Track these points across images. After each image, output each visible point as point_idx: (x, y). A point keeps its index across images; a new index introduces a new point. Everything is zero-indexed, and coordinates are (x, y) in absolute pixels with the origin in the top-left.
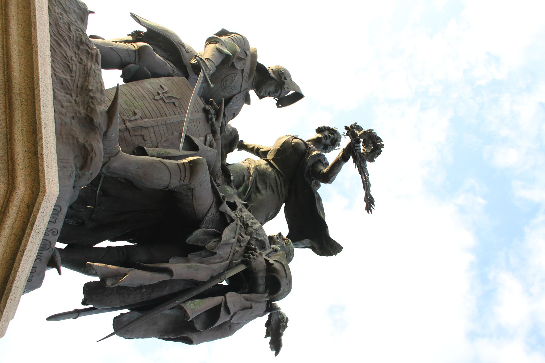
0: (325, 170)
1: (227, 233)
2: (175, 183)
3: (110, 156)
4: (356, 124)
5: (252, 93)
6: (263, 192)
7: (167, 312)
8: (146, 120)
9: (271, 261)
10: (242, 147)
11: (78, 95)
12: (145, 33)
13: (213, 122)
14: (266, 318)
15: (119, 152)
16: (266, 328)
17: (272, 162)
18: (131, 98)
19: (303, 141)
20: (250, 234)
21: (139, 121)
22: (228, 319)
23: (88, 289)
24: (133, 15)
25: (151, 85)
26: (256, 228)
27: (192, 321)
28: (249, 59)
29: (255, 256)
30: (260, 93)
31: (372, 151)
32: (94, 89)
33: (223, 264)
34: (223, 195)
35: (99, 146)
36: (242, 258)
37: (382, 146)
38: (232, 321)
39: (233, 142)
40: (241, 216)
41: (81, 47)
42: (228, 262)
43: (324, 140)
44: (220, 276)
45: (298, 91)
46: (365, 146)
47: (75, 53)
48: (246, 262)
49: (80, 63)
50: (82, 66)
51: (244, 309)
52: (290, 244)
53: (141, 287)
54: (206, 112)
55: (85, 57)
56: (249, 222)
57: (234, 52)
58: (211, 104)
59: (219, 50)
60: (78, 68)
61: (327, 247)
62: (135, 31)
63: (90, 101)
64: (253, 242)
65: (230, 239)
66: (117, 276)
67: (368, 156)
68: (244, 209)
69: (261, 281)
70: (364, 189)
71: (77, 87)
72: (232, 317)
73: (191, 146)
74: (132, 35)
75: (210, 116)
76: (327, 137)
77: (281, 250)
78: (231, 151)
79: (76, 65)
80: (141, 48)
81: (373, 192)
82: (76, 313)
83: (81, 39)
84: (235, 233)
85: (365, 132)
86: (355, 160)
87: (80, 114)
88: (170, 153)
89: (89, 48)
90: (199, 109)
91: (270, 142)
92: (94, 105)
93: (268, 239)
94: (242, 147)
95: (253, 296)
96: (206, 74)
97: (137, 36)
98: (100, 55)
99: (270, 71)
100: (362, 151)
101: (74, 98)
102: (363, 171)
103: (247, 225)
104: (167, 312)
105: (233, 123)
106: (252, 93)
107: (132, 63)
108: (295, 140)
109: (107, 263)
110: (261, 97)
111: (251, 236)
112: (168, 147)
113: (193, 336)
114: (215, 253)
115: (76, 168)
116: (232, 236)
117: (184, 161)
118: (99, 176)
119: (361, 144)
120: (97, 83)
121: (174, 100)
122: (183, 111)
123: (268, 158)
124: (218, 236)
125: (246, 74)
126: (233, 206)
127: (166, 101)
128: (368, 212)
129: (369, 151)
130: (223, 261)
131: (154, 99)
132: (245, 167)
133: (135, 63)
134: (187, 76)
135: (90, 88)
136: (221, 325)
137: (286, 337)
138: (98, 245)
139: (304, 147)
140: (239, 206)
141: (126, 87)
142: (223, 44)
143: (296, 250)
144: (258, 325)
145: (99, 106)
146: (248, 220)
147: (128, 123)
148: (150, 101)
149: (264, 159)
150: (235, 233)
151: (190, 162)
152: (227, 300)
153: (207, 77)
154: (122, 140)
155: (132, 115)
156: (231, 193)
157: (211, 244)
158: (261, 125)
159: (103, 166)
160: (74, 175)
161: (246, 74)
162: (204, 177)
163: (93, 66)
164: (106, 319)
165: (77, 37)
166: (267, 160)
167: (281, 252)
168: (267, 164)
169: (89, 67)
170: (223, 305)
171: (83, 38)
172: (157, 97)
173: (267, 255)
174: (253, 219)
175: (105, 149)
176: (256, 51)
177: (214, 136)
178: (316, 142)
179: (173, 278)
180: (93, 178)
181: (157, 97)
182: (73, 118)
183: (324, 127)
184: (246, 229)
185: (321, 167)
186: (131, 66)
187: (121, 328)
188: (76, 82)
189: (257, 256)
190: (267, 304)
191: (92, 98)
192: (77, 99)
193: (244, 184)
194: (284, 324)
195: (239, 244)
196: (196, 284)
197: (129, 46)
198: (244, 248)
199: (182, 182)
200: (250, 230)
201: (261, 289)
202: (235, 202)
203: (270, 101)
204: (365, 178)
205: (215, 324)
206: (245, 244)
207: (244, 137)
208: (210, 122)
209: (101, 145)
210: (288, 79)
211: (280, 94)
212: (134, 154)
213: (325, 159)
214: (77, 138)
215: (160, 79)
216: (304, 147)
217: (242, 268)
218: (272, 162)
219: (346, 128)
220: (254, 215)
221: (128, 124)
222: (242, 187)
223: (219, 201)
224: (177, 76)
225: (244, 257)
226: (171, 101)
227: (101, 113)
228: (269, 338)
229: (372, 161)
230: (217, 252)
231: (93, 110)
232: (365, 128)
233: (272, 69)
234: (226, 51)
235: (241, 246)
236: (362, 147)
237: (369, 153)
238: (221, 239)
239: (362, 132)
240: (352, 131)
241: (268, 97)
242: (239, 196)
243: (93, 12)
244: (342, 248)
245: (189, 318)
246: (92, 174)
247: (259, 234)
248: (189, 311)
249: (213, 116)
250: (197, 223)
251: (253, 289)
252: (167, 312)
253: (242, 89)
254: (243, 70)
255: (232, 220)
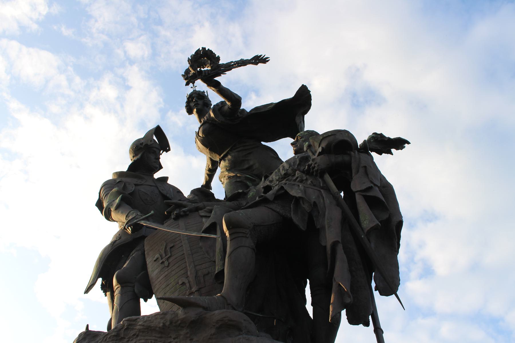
0: (228, 103)
1: (295, 192)
2: (249, 242)
3: (226, 303)
4: (183, 75)
5: (157, 175)
6: (251, 163)
7: (373, 245)
8: (189, 273)
9: (320, 150)
10: (208, 185)
11: (169, 336)
12: (103, 280)
13: (188, 211)
14: (374, 154)
15: (221, 296)
16: (383, 154)
17: (222, 156)
18: (168, 289)
19: (201, 126)
20: (294, 171)
21: (191, 280)
22: (377, 189)
23: (353, 320)
24: (87, 292)
25: (154, 270)
26: (288, 166)
27: (380, 222)
28: (124, 179)
29: (316, 165)
30: (156, 168)
31: (209, 58)
32: (162, 321)
33: (324, 195)
34: (257, 199)
35: (217, 314)
36: (318, 177)
37: (204, 49)
38: (379, 185)
39: (204, 193)
40: (277, 180)
41: (122, 336)
42: (322, 190)
43: (199, 107)
44: (336, 198)
45: (153, 131)
46: (205, 65)
47: (128, 341)
48: (321, 174)
49: (137, 336)
50: (141, 334)
51: (366, 173)
52: (302, 134)
53: (351, 271)
54: (178, 217)
55: (132, 332)
56: (283, 172)
57: (118, 193)
58: (170, 213)
59: (117, 208)
60: (142, 338)
61: (303, 99)
62: (102, 290)
63: (174, 324)
64: (302, 168)
65: (300, 190)
66: (341, 293)
67: (214, 63)
68: (270, 178)
69: (340, 158)
70: (246, 65)
71: (161, 337)
72: (375, 185)
73: (213, 228)
74: (105, 292)
75: (182, 213)
76: (196, 103)
77: (309, 142)
78: (213, 195)
79: (140, 340)
80: (119, 281)
81: (249, 56)
82: (378, 332)
83: (114, 336)
84: (294, 185)
85: (191, 66)
86: (219, 75)
87: (187, 333)
88: (220, 249)
89: (122, 328)
90: (175, 224)
91: (201, 161)
92: (178, 321)
93: (298, 155)
94: (208, 185)
95: (354, 166)
96: (142, 218)
97: (107, 288)
98: (129, 318)
99: (135, 158)
100: (209, 69)
101: (172, 340)
102: (229, 67)
103: (285, 174)
104: (373, 245)
105: (186, 193)
106: (157, 175)
107: (134, 290)
108: (201, 134)
109: (329, 303)
110: (161, 167)
111: (296, 170)
112: (214, 251)
113: (395, 220)
114: (315, 202)
115: (240, 334)
116: (297, 188)
117: (227, 234)
118: (245, 313)
119: (202, 69)
120: (156, 318)
121: (168, 248)
122: (178, 239)
123: (218, 160)
124: (297, 200)
125: (139, 182)
126: (267, 189)
127: (169, 255)
128: (268, 61)
129: (209, 61)
130: (322, 195)
131: (168, 266)
132: (228, 181)
133: (134, 287)
134: (143, 237)
135: (161, 325)
136: (384, 195)
137: (391, 134)
138: (311, 315)
139: (207, 125)
140: (267, 183)
141: (158, 294)
142: (110, 204)
143: (306, 129)
144: (381, 161)
145: (179, 315)
146: (281, 174)
147: (193, 290)
148: (170, 270)
149: (220, 163)
150: (294, 185)
151: (228, 228)
152: (359, 189)
153: (144, 217)
154: (210, 293)
155: (184, 287)
156: (254, 192)
157: (306, 207)
158: (185, 168)
159: (235, 310)
160: (247, 336)
161: (139, 182)
162: (241, 215)
163: (140, 323)
164: (383, 303)
165: (113, 340)
166: (221, 160)
167: (311, 141)
168: (225, 160)
169: (142, 327)
170: (364, 194)
171: (113, 334)
172: (166, 263)
173: (314, 154)
174: (279, 169)
175: (220, 309)
176: (116, 173)
177: (201, 209)
178: (201, 115)
179: (340, 240)
180: (248, 319)
181: (166, 263)
182: (191, 340)
183: (186, 107)
184: (289, 175)
185: (226, 107)
186: (136, 291)
187: (390, 287)
188: (157, 338)
189: (316, 163)
190: (362, 152)
191: (171, 323)
192: (173, 337)
193: (245, 181)
194: (379, 136)
195: (304, 181)
196: (345, 221)
197: (117, 293)
198: (308, 176)
199: (248, 236)
200: (290, 171)
201: (346, 158)
202: (264, 188)
203: (164, 158)
204: (235, 64)
205: (383, 200)
206: (304, 175)
207: (200, 182)
208: (188, 213)
209: (216, 312)
210: (143, 141)
211: (157, 148)
212: (223, 282)
213: (217, 105)
214: (211, 335)
215: (147, 262)
216: (207, 125)
217: (327, 177)
218: (222, 156)
219: (187, 84)
220: (277, 168)
221: (194, 289)
222: (248, 183)
223: (264, 201)
224: (144, 246)
225: (316, 175)
226: (169, 250)
227: (186, 313)
228: (393, 150)
229: (218, 59)
230: (313, 201)
231: (183, 321)
232: (187, 65)
233: (133, 157)
234: (117, 201)
235: (307, 180)
236: (206, 69)
237: (211, 61)
238: (300, 197)
239: (191, 69)
240: (189, 78)
241: (160, 160)
242: (256, 184)
243: (88, 326)
244: (303, 85)
245: (378, 224)
246: (245, 320)
247: (294, 163)
248: (372, 225)
249: (181, 210)
250: (286, 222)
251: (348, 166)
252: (372, 245)
253: (155, 185)
254: (136, 185)
255: (282, 188)
